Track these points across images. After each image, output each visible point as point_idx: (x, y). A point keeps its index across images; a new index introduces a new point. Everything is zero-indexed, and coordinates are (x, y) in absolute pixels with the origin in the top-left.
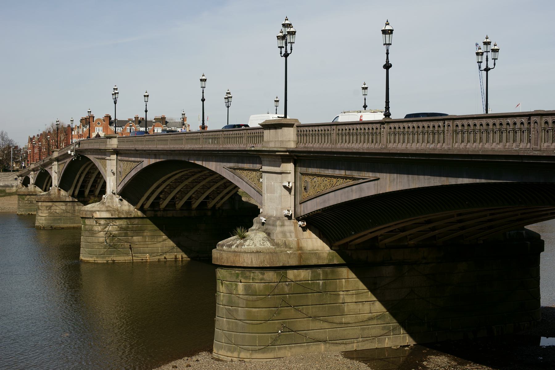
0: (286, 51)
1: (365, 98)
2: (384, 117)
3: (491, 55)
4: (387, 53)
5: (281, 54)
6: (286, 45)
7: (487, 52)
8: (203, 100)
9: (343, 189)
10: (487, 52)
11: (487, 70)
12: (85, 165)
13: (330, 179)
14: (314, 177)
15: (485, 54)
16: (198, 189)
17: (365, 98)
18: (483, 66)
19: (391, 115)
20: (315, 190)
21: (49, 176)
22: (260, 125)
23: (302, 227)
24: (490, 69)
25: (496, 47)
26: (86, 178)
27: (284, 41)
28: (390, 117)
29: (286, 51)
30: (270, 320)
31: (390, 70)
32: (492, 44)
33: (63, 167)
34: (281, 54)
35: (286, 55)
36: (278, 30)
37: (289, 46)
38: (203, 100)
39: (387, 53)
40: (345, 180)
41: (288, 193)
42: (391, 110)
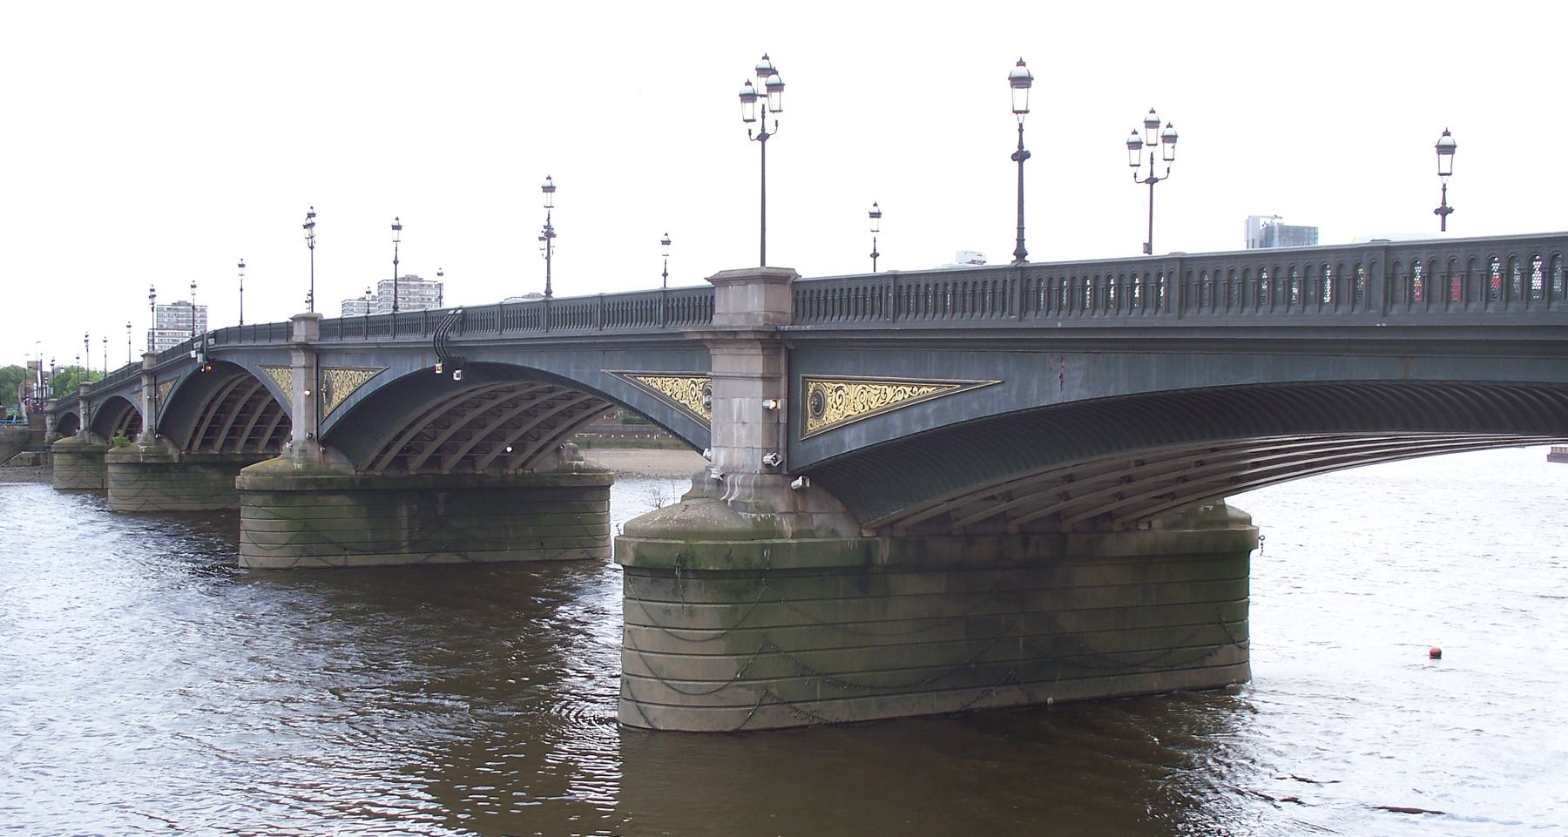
2: (1014, 258)
8: (396, 262)
11: (1152, 181)
12: (221, 384)
13: (879, 387)
14: (837, 386)
16: (424, 428)
18: (1144, 174)
19: (1027, 254)
20: (841, 412)
21: (280, 415)
22: (708, 280)
23: (702, 474)
24: (1157, 180)
26: (237, 423)
28: (1027, 258)
30: (738, 629)
32: (1163, 126)
33: (167, 390)
38: (396, 262)
40: (915, 389)
42: (1027, 246)
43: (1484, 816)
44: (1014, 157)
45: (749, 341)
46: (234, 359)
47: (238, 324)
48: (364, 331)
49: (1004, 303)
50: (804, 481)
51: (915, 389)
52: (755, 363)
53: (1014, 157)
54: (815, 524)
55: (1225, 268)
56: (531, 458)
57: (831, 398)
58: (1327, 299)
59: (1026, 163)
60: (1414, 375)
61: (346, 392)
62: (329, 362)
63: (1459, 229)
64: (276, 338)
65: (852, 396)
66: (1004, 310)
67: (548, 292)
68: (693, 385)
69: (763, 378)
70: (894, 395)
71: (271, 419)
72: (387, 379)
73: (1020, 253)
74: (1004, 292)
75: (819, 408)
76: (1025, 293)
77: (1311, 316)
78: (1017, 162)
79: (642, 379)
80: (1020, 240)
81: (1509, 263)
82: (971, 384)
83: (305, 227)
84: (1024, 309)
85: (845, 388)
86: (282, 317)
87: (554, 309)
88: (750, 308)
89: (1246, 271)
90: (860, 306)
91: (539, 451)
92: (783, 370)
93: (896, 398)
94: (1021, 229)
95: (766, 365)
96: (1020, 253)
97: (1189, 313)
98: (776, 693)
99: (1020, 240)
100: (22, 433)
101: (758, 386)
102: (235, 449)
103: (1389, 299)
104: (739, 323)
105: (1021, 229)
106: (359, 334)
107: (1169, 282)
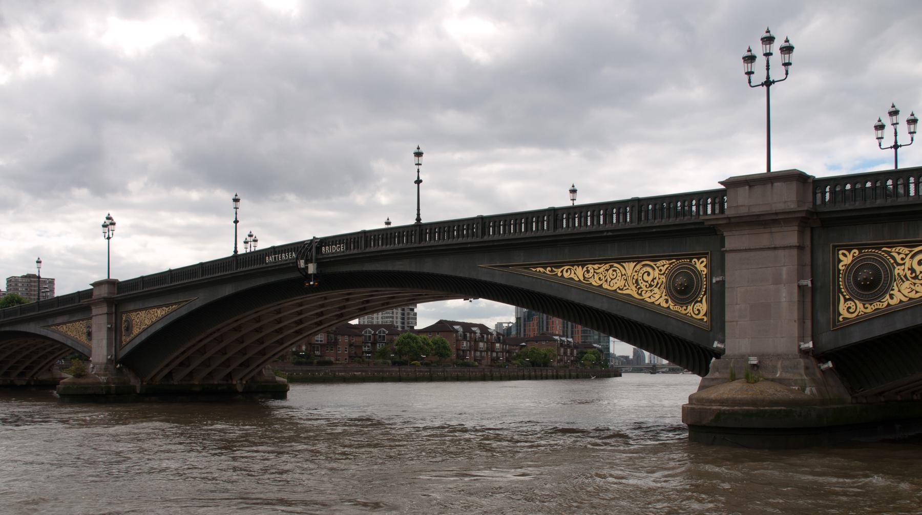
0: (109, 236)
1: (418, 170)
2: (416, 221)
3: (253, 244)
4: (236, 214)
5: (105, 237)
6: (109, 232)
7: (251, 242)
9: (234, 243)
10: (251, 242)
11: (768, 83)
15: (249, 243)
17: (418, 170)
24: (774, 82)
25: (256, 239)
27: (107, 229)
28: (421, 221)
29: (109, 236)
31: (238, 224)
32: (254, 236)
34: (105, 237)
35: (109, 238)
36: (103, 220)
37: (111, 232)
39: (236, 214)
41: (92, 283)
42: (421, 216)
44: (416, 182)
47: (231, 254)
49: (358, 245)
51: (171, 307)
52: (104, 309)
53: (416, 182)
56: (37, 372)
59: (421, 184)
60: (270, 281)
63: (581, 200)
66: (358, 248)
68: (81, 325)
69: (107, 314)
70: (160, 313)
72: (184, 312)
73: (418, 219)
74: (358, 241)
75: (129, 329)
76: (366, 241)
78: (417, 185)
79: (54, 327)
80: (418, 214)
82: (188, 301)
83: (421, 164)
84: (366, 246)
85: (141, 314)
86: (85, 285)
89: (355, 238)
90: (250, 263)
91: (40, 369)
92: (114, 310)
93: (162, 314)
94: (418, 210)
96: (418, 219)
99: (418, 214)
105: (418, 210)
107: (415, 233)
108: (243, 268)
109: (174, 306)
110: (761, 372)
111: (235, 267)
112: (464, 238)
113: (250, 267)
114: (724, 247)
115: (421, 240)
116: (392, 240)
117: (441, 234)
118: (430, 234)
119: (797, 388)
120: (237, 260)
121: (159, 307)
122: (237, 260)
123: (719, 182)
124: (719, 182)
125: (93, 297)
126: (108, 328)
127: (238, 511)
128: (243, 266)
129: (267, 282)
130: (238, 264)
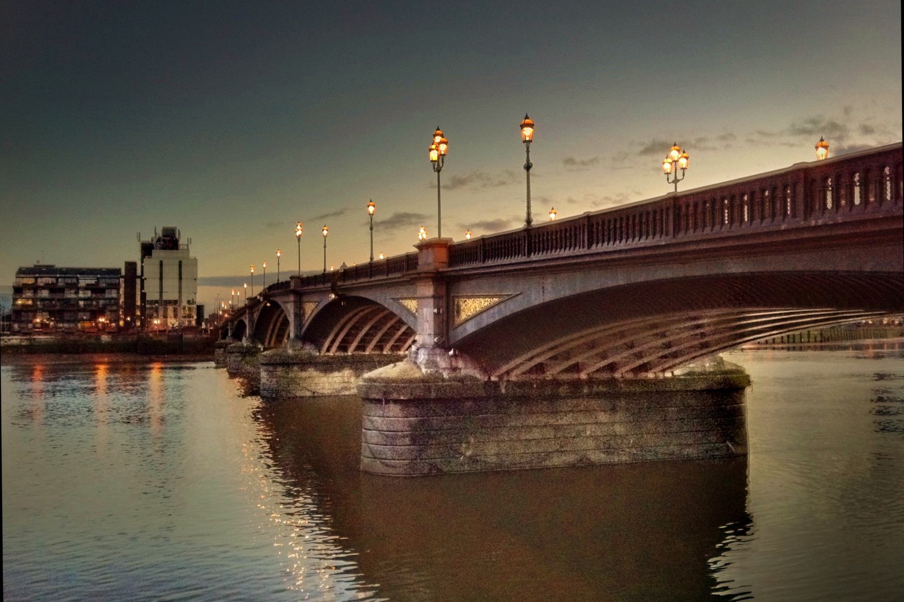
41: (346, 263)
42: (532, 216)
43: (728, 562)
45: (427, 278)
46: (363, 294)
48: (369, 274)
50: (455, 351)
54: (462, 374)
55: (682, 202)
57: (463, 306)
58: (829, 205)
61: (309, 312)
62: (305, 299)
64: (392, 273)
65: (470, 304)
67: (325, 270)
71: (356, 335)
73: (372, 259)
77: (737, 230)
81: (774, 190)
87: (535, 237)
88: (430, 261)
95: (435, 290)
96: (372, 259)
97: (594, 246)
98: (625, 559)
100: (207, 338)
101: (431, 301)
102: (347, 352)
103: (537, 249)
104: (426, 269)
106: (518, 252)
108: (695, 229)
109: (495, 299)
110: (226, 308)
111: (672, 230)
112: (765, 221)
113: (708, 230)
114: (120, 270)
115: (809, 210)
116: (717, 214)
117: (756, 208)
118: (731, 208)
119: (275, 545)
120: (530, 236)
121: (485, 297)
122: (530, 236)
123: (414, 246)
124: (414, 246)
125: (419, 267)
126: (435, 313)
127: (204, 584)
128: (655, 229)
129: (761, 269)
130: (592, 232)
